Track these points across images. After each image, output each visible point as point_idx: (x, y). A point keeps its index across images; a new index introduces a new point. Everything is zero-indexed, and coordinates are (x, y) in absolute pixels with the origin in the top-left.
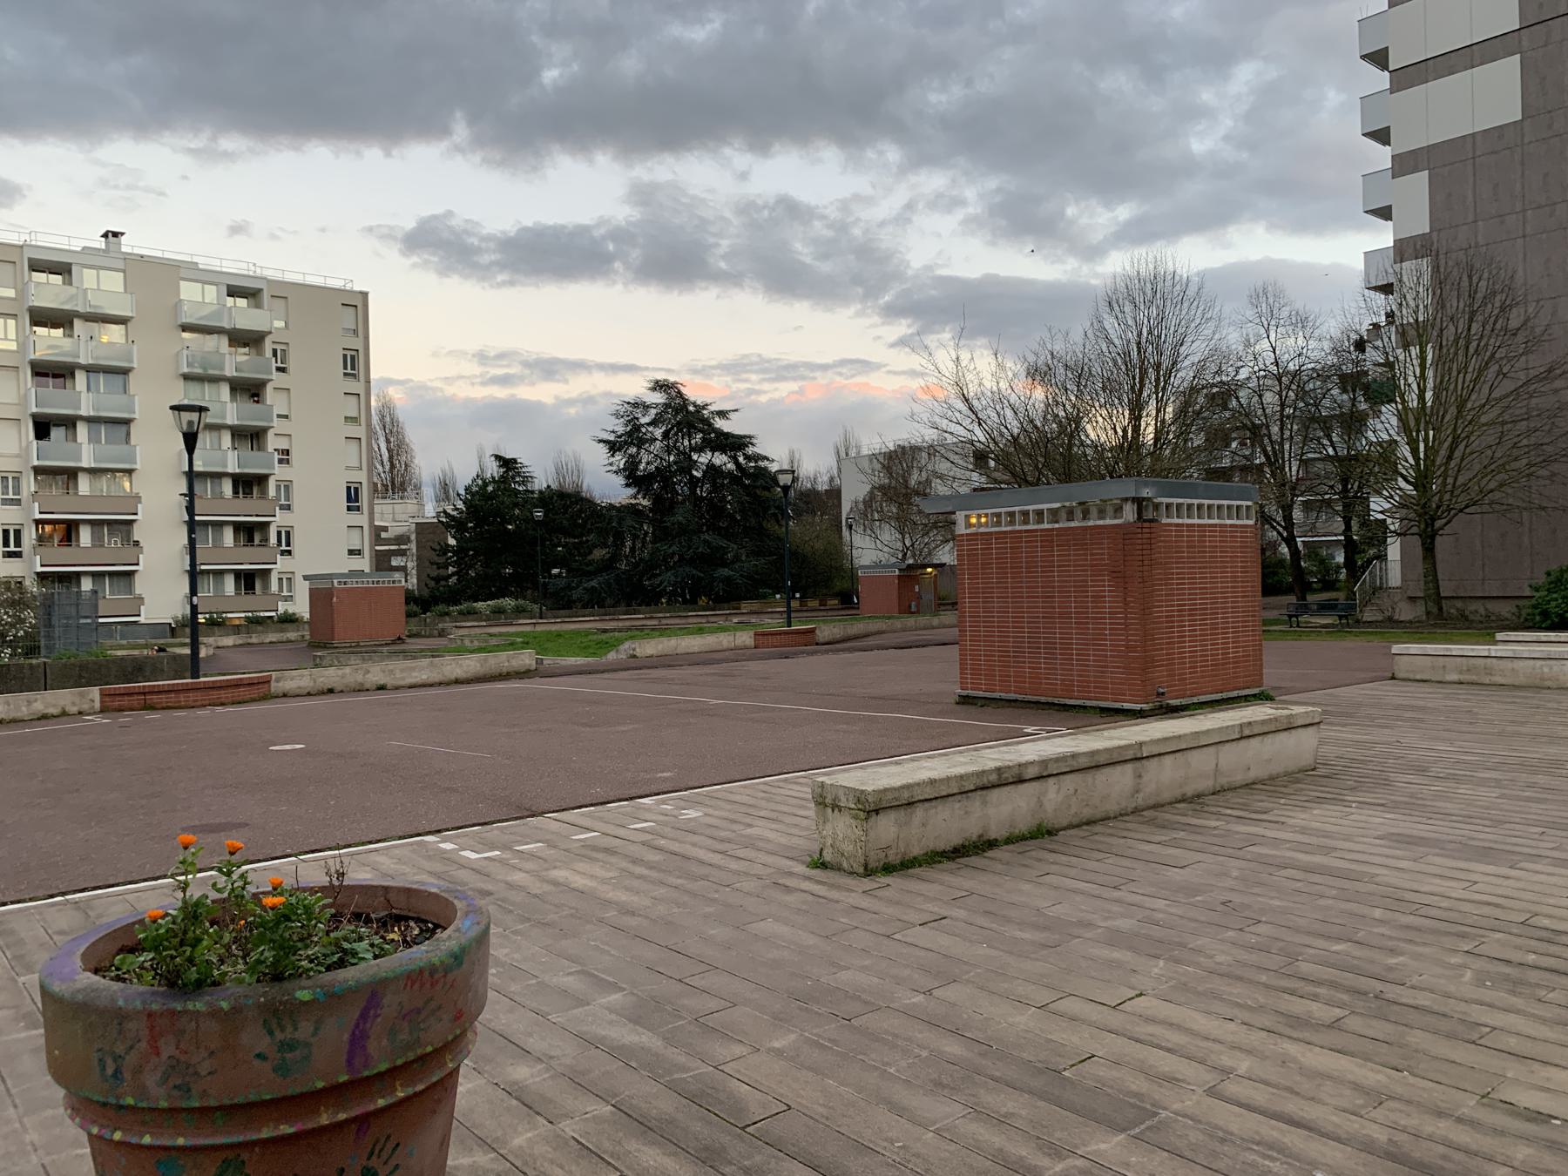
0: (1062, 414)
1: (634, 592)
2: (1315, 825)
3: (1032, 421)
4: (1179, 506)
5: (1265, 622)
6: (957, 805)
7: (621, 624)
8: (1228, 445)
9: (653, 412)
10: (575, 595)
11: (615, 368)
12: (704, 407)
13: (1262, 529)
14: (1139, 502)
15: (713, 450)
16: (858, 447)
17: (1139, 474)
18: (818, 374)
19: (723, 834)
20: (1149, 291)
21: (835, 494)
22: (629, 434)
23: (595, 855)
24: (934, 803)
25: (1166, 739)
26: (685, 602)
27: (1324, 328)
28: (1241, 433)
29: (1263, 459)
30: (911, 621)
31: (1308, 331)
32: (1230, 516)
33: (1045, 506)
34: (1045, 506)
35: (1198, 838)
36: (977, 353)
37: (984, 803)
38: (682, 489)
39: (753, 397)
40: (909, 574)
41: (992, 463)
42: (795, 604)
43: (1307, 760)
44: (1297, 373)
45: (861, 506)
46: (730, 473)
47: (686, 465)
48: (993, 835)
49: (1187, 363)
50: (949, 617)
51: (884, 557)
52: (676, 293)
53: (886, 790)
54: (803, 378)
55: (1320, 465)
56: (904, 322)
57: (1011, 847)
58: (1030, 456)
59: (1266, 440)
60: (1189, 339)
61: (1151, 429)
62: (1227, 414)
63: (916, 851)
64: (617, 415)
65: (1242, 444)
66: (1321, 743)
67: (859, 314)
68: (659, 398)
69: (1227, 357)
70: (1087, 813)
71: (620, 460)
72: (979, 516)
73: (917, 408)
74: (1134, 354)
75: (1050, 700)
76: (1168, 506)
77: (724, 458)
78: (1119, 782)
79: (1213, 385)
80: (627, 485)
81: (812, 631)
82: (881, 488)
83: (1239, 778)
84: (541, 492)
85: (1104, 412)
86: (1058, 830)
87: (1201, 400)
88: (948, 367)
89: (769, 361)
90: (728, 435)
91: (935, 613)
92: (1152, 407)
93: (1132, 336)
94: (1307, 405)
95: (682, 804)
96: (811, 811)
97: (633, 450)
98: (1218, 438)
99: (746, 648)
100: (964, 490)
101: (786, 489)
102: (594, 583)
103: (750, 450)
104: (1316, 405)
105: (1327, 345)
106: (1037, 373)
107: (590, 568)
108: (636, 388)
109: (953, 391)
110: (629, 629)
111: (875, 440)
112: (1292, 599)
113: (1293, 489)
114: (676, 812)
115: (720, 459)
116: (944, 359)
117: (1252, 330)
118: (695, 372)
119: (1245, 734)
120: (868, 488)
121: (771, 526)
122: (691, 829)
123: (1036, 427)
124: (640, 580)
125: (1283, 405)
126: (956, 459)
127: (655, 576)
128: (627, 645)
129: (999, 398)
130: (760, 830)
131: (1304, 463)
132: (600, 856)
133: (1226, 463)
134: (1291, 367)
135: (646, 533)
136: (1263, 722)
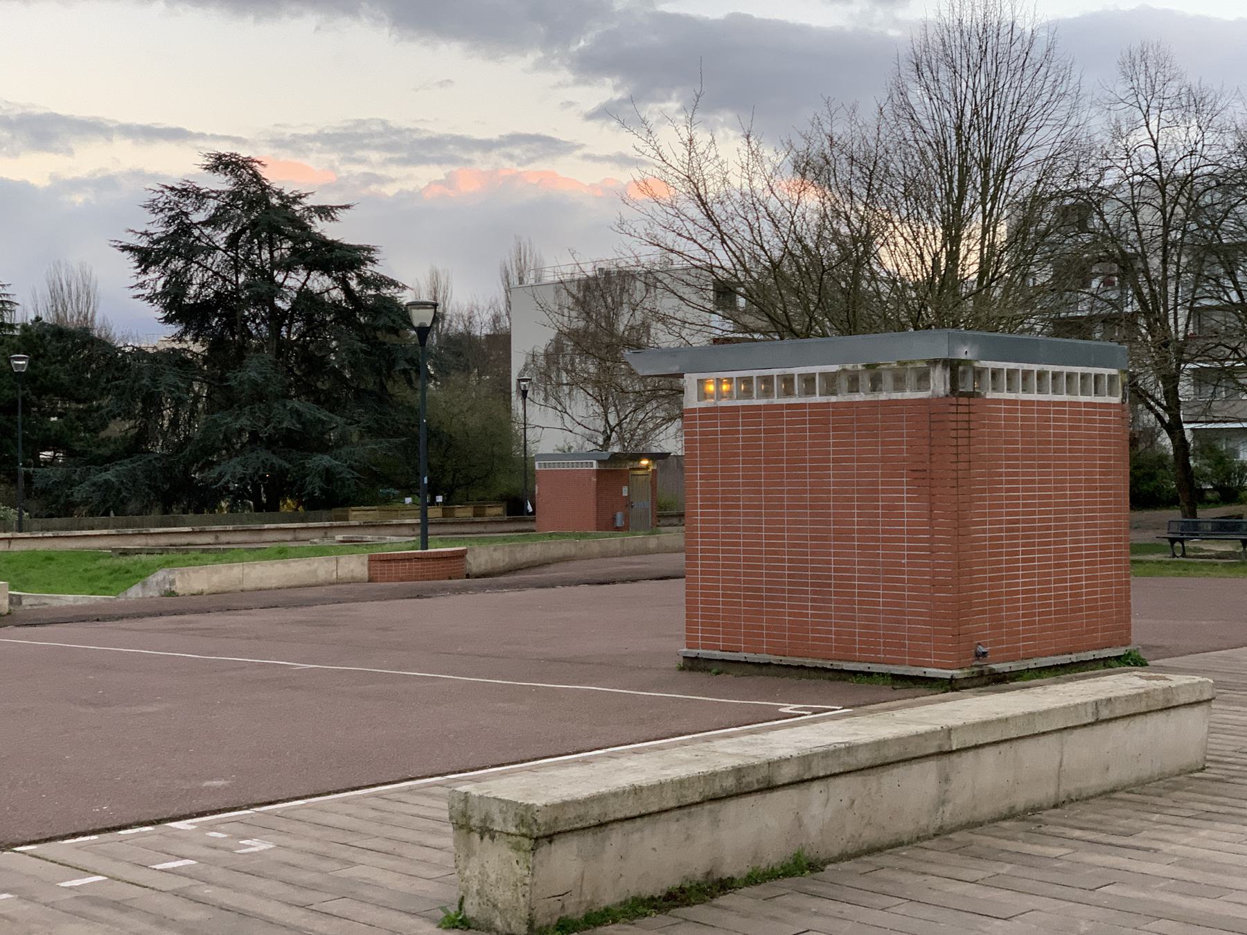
0: (844, 230)
1: (178, 491)
2: (1200, 853)
3: (800, 240)
4: (1011, 373)
5: (1136, 549)
6: (674, 827)
7: (152, 542)
8: (1086, 284)
9: (212, 204)
10: (78, 494)
11: (150, 134)
12: (296, 199)
13: (1134, 410)
14: (953, 366)
15: (310, 268)
16: (539, 271)
17: (955, 326)
18: (477, 155)
19: (306, 877)
20: (975, 50)
21: (501, 341)
22: (172, 238)
23: (96, 911)
24: (639, 822)
25: (986, 724)
26: (259, 507)
27: (1227, 114)
28: (1106, 267)
29: (1137, 306)
30: (614, 542)
31: (1205, 117)
32: (1069, 393)
33: (816, 369)
34: (816, 369)
35: (1035, 874)
36: (719, 135)
37: (715, 822)
38: (259, 329)
39: (373, 187)
40: (613, 468)
41: (742, 302)
42: (434, 513)
43: (1192, 756)
44: (1187, 180)
45: (541, 361)
46: (335, 305)
47: (265, 290)
48: (727, 871)
49: (1028, 159)
50: (672, 536)
51: (576, 441)
52: (251, 18)
53: (565, 804)
54: (452, 160)
55: (1218, 317)
56: (608, 81)
57: (754, 890)
58: (797, 292)
59: (1142, 278)
60: (1032, 124)
61: (974, 257)
62: (1086, 238)
63: (609, 898)
64: (153, 207)
65: (1107, 283)
66: (1211, 731)
67: (540, 66)
68: (222, 183)
69: (1087, 152)
70: (870, 836)
71: (156, 279)
72: (719, 382)
73: (627, 213)
74: (952, 143)
75: (819, 663)
76: (995, 373)
77: (327, 281)
78: (914, 791)
79: (1067, 194)
80: (168, 320)
81: (461, 556)
82: (573, 334)
83: (1094, 782)
84: (25, 327)
85: (906, 231)
86: (825, 863)
87: (1048, 216)
88: (676, 153)
89: (398, 132)
90: (332, 246)
91: (653, 530)
92: (975, 226)
93: (949, 117)
94: (1201, 226)
95: (241, 829)
96: (448, 839)
97: (178, 264)
98: (1073, 273)
99: (354, 581)
100: (699, 341)
101: (423, 332)
102: (109, 475)
103: (368, 270)
104: (1215, 228)
105: (1231, 141)
106: (813, 169)
107: (103, 451)
108: (185, 165)
109: (683, 189)
110: (163, 550)
111: (569, 260)
112: (1175, 514)
113: (1180, 351)
114: (231, 843)
115: (319, 282)
116: (671, 139)
117: (1122, 112)
118: (279, 143)
119: (1102, 717)
120: (552, 334)
121: (398, 389)
122: (254, 870)
123: (805, 247)
124: (186, 472)
125: (1166, 226)
126: (687, 292)
127: (211, 464)
128: (160, 575)
129: (753, 203)
130: (367, 869)
131: (1196, 313)
132: (104, 913)
133: (1083, 310)
134: (1180, 170)
135: (198, 397)
136: (1129, 699)
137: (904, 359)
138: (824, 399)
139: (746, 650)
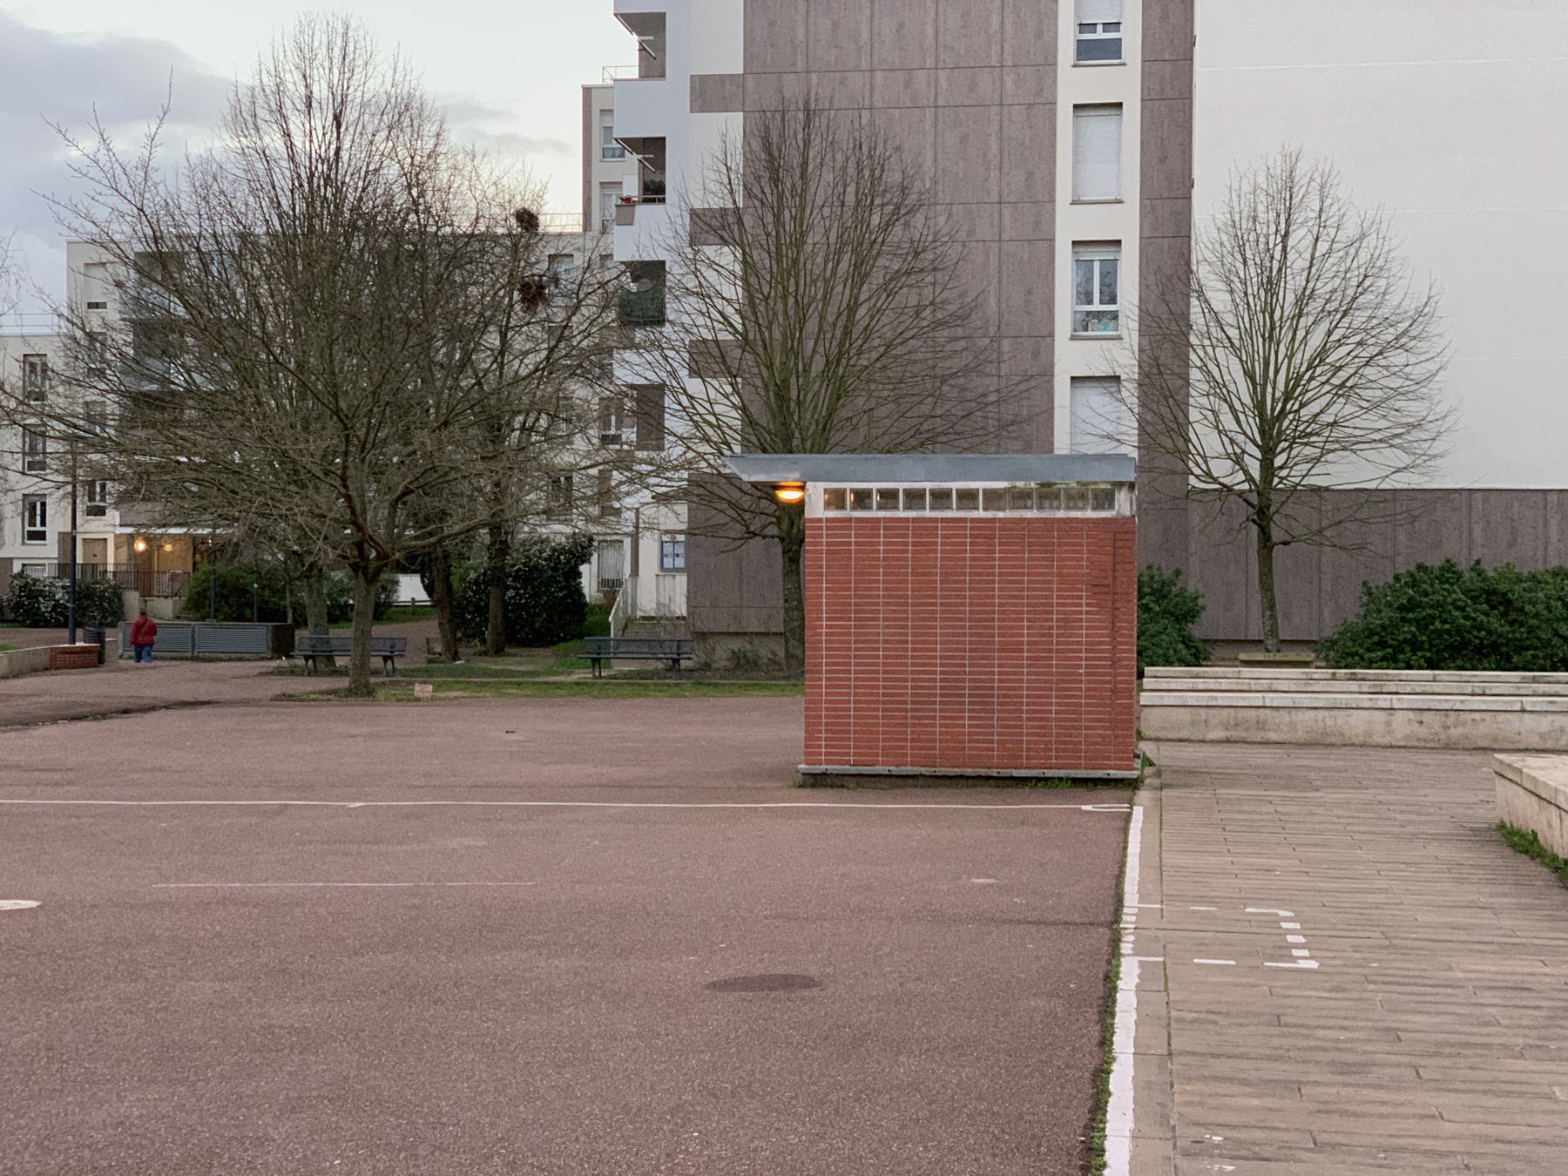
75: (983, 772)
137: (1085, 480)
138: (989, 514)
139: (913, 764)
